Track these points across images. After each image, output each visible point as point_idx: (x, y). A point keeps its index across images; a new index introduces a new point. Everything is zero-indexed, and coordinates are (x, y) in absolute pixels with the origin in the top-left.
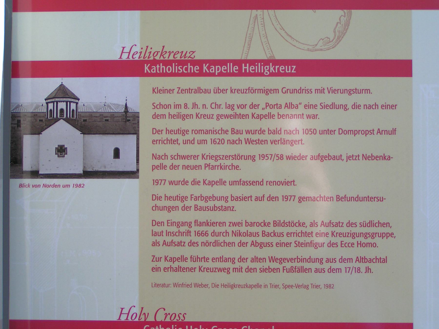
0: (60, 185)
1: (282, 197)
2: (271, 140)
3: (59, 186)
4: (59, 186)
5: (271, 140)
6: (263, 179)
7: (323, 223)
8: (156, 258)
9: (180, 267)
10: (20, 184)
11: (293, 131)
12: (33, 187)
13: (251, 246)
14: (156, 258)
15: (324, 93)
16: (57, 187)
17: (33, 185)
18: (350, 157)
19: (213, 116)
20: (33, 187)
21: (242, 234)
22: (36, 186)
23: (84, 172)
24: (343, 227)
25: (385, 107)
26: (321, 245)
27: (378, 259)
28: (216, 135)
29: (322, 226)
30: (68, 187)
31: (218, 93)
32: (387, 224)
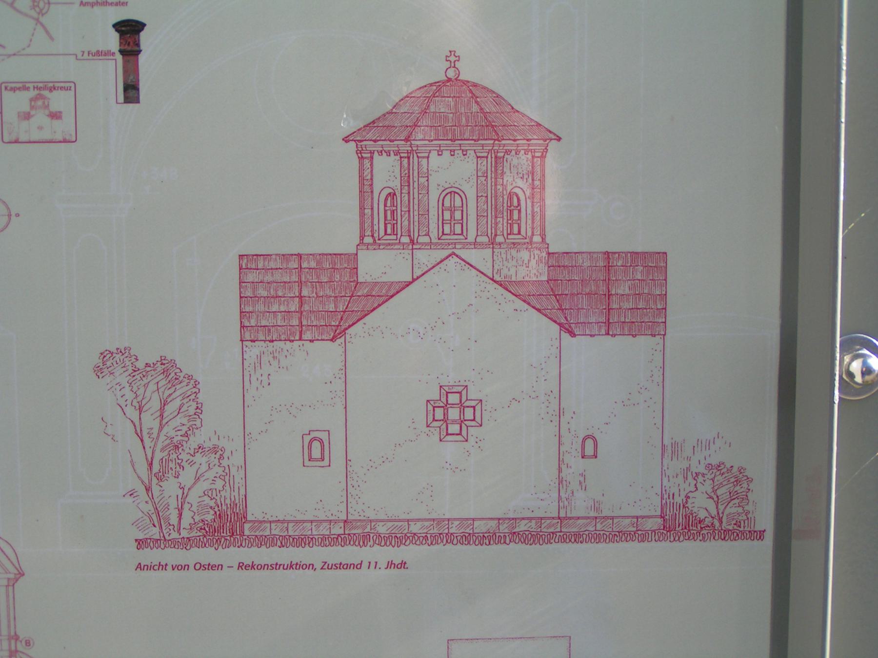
0: (188, 566)
1: (368, 564)
2: (172, 566)
3: (220, 567)
4: (220, 567)
5: (172, 566)
6: (362, 562)
7: (141, 566)
8: (328, 565)
9: (404, 562)
10: (240, 563)
11: (154, 566)
12: (173, 569)
13: (136, 570)
14: (328, 565)
15: (166, 570)
16: (216, 568)
17: (174, 566)
18: (248, 566)
19: (323, 566)
20: (173, 569)
21: (255, 567)
22: (180, 568)
23: (64, 140)
24: (323, 562)
25: (679, 494)
26: (287, 566)
27: (163, 566)
28: (273, 570)
29: (138, 569)
30: (162, 569)
31: (347, 564)
32: (389, 562)
